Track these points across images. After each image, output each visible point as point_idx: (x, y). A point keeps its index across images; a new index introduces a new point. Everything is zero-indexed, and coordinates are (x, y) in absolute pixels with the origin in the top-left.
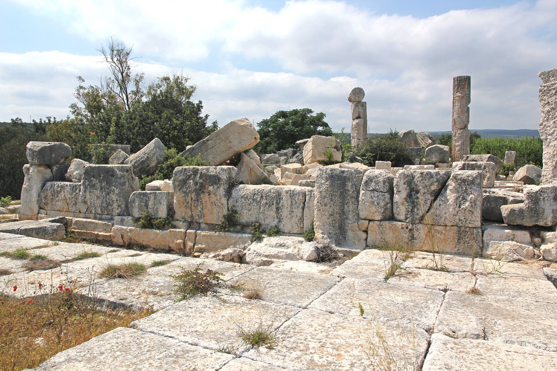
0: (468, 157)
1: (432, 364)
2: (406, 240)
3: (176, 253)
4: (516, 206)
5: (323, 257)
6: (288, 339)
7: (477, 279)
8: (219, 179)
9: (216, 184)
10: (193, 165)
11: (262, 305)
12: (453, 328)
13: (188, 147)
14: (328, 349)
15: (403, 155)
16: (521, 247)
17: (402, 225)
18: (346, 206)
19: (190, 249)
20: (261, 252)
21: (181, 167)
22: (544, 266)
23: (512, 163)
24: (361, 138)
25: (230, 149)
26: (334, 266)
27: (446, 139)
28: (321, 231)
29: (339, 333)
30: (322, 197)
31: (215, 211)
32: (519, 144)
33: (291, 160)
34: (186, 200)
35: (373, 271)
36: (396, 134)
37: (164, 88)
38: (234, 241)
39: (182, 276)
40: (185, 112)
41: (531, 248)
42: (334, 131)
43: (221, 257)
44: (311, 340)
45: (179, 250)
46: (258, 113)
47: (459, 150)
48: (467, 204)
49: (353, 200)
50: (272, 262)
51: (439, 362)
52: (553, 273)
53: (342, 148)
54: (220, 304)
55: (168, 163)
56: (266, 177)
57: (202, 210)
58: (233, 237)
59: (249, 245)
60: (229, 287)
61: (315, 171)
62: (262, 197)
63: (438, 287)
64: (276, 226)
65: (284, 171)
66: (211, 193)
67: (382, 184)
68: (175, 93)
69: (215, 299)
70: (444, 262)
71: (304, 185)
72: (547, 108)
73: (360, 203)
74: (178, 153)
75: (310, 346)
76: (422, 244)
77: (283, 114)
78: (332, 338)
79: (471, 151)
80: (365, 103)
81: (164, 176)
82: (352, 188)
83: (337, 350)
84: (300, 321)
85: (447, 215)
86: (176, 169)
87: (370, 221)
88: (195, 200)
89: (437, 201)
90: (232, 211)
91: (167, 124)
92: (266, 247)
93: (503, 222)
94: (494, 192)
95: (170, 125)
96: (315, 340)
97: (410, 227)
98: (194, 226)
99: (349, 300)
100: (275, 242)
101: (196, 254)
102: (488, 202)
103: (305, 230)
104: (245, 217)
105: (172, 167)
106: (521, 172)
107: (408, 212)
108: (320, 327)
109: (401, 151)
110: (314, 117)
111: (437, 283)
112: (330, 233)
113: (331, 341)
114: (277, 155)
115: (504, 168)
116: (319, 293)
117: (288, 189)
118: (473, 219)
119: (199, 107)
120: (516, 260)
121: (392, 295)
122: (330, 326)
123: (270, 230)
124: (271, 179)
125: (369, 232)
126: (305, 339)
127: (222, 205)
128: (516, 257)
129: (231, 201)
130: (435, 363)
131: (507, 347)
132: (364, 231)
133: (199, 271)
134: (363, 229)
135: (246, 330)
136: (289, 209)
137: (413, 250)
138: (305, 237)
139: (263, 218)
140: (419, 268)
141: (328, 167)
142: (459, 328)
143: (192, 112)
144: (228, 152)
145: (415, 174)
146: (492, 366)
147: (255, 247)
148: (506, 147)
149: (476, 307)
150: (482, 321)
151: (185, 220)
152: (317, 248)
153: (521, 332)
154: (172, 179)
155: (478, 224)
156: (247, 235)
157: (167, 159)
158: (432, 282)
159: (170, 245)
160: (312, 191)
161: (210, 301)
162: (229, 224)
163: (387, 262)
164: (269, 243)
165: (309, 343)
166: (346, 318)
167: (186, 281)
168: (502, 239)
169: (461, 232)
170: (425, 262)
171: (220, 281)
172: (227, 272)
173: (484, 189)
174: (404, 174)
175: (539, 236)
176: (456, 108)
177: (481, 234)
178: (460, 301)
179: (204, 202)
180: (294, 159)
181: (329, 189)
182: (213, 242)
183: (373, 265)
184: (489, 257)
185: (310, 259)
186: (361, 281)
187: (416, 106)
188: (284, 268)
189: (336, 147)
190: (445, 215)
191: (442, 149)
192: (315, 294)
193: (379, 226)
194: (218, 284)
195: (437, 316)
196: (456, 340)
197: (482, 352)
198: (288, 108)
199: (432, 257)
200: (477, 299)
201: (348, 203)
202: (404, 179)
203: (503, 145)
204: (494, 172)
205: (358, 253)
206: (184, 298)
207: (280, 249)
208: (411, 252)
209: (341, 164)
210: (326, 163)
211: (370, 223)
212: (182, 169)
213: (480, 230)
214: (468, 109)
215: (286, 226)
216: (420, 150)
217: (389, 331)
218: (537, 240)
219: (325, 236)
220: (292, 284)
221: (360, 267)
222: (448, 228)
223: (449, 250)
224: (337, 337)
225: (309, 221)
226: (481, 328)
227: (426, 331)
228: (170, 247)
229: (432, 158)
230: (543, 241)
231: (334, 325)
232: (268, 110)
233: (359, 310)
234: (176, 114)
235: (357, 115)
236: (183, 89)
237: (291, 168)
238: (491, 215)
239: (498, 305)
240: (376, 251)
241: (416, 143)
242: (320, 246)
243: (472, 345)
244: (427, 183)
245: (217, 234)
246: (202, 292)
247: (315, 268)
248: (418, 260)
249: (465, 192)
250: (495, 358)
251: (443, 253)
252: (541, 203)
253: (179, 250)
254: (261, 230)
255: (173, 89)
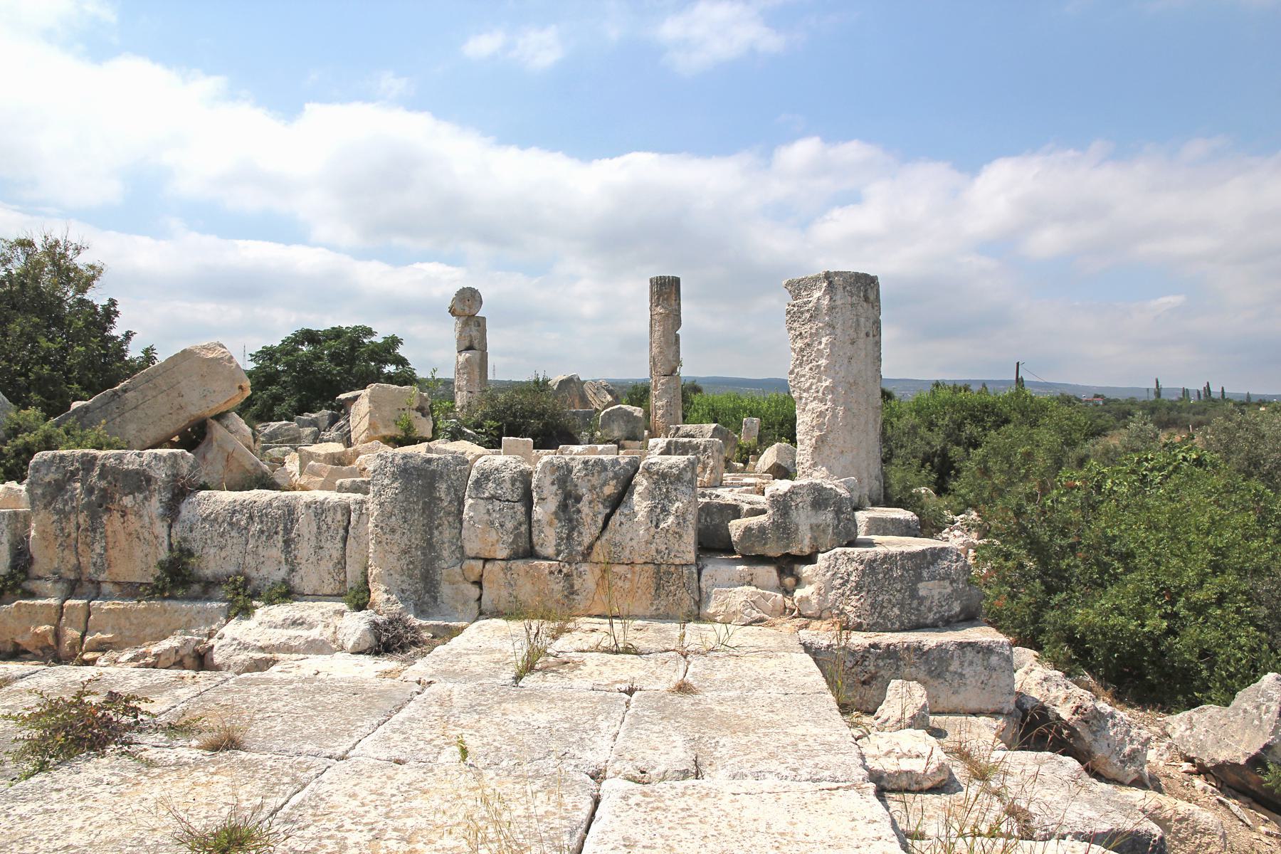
0: (678, 429)
1: (601, 841)
2: (559, 596)
3: (35, 657)
4: (754, 521)
5: (388, 642)
6: (299, 833)
7: (689, 663)
8: (149, 480)
9: (139, 489)
10: (86, 447)
11: (242, 761)
12: (641, 765)
13: (76, 405)
14: (389, 843)
15: (557, 425)
16: (763, 596)
17: (550, 566)
18: (436, 533)
19: (72, 646)
20: (249, 639)
21: (50, 453)
22: (801, 628)
23: (753, 440)
24: (477, 389)
25: (181, 412)
26: (411, 661)
27: (639, 395)
28: (383, 588)
29: (415, 804)
30: (385, 515)
31: (138, 553)
32: (765, 405)
33: (326, 435)
34: (62, 530)
35: (492, 665)
36: (545, 382)
37: (16, 267)
38: (185, 619)
39: (39, 715)
40: (71, 322)
41: (780, 596)
42: (420, 374)
43: (149, 660)
44: (353, 827)
45: (42, 649)
46: (247, 334)
47: (663, 416)
48: (671, 519)
49: (451, 519)
50: (275, 662)
51: (613, 836)
52: (814, 639)
53: (432, 411)
54: (139, 771)
55: (19, 441)
56: (264, 473)
57: (106, 550)
58: (182, 610)
59: (222, 626)
60: (164, 729)
61: (371, 457)
62: (251, 517)
63: (618, 686)
64: (284, 581)
65: (305, 459)
66: (128, 511)
67: (508, 485)
68: (46, 280)
69: (126, 759)
70: (631, 634)
71: (348, 490)
72: (800, 344)
73: (465, 524)
74: (46, 419)
75: (350, 842)
76: (589, 603)
77: (309, 336)
78: (399, 817)
79: (684, 417)
80: (484, 319)
81: (5, 473)
82: (448, 494)
83: (409, 843)
84: (330, 787)
85: (634, 543)
86: (37, 457)
87: (486, 560)
88: (87, 530)
89: (616, 518)
90: (181, 550)
91: (24, 348)
92: (261, 629)
93: (735, 553)
94: (718, 496)
95: (32, 352)
96: (360, 828)
97: (565, 570)
98: (84, 591)
99: (439, 731)
100: (282, 617)
101: (88, 656)
102: (707, 514)
103: (348, 586)
104: (212, 564)
105: (29, 451)
106: (769, 457)
107: (562, 539)
108: (374, 797)
109: (552, 416)
110: (377, 345)
111: (615, 678)
112: (403, 591)
113: (396, 824)
114: (295, 424)
115: (741, 449)
116: (375, 722)
117: (310, 499)
118: (682, 548)
119: (110, 313)
120: (756, 621)
121: (528, 711)
122: (395, 792)
123: (270, 590)
124: (278, 477)
125: (485, 584)
126: (339, 828)
127: (156, 537)
128: (755, 615)
129: (177, 528)
130: (606, 840)
131: (734, 786)
132: (474, 583)
133: (86, 699)
134: (473, 578)
135: (198, 825)
136: (313, 543)
137: (571, 616)
138: (349, 602)
139: (253, 564)
140: (583, 651)
141: (397, 450)
142: (652, 763)
143: (88, 325)
144: (174, 417)
145: (573, 464)
146: (705, 827)
147: (235, 629)
148: (745, 411)
149: (685, 717)
150: (693, 742)
151: (60, 578)
152: (375, 625)
153: (759, 755)
154: (26, 481)
155: (691, 557)
156: (215, 605)
157: (14, 432)
158: (608, 676)
159: (18, 640)
160: (363, 502)
161: (113, 768)
162: (172, 581)
163: (518, 645)
164: (268, 619)
165: (347, 835)
166: (432, 770)
167: (49, 726)
168: (732, 583)
169: (662, 574)
170: (593, 639)
171: (140, 717)
172: (161, 693)
173: (699, 490)
174: (551, 463)
175: (792, 575)
176: (657, 335)
177: (695, 576)
178: (656, 709)
179: (109, 533)
180: (333, 433)
181: (400, 497)
182: (131, 624)
183: (492, 651)
184: (711, 619)
185: (359, 649)
186: (465, 687)
187: (579, 329)
188: (300, 672)
189: (420, 409)
190: (630, 544)
191: (630, 414)
192: (366, 725)
193: (506, 570)
194: (137, 723)
195: (612, 744)
196: (646, 788)
197: (690, 803)
198: (322, 322)
199: (607, 627)
200: (686, 702)
201: (440, 525)
202: (553, 473)
203: (740, 407)
204: (721, 458)
205: (463, 629)
206: (43, 767)
207: (293, 632)
208: (569, 621)
209: (431, 444)
210: (399, 442)
211: (487, 566)
212: (54, 456)
213: (694, 569)
214: (677, 337)
215: (306, 578)
216: (590, 415)
217: (518, 786)
218: (789, 581)
219: (394, 597)
220: (314, 708)
221: (465, 659)
222: (637, 568)
223: (639, 611)
224: (408, 813)
225: (357, 566)
226: (690, 756)
227: (592, 777)
228: (17, 645)
229: (612, 431)
230: (798, 582)
231: (403, 789)
232: (278, 325)
233: (457, 749)
234: (49, 327)
235: (467, 344)
236: (68, 269)
237: (323, 453)
238: (713, 543)
239: (722, 709)
240: (500, 622)
241: (584, 401)
242: (380, 619)
243: (673, 792)
244: (595, 480)
245: (143, 604)
246: (91, 748)
247: (370, 667)
248: (585, 634)
249: (667, 497)
250: (713, 810)
251: (629, 617)
252: (793, 513)
253: (42, 649)
254: (248, 592)
255: (42, 270)
